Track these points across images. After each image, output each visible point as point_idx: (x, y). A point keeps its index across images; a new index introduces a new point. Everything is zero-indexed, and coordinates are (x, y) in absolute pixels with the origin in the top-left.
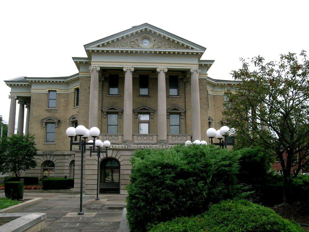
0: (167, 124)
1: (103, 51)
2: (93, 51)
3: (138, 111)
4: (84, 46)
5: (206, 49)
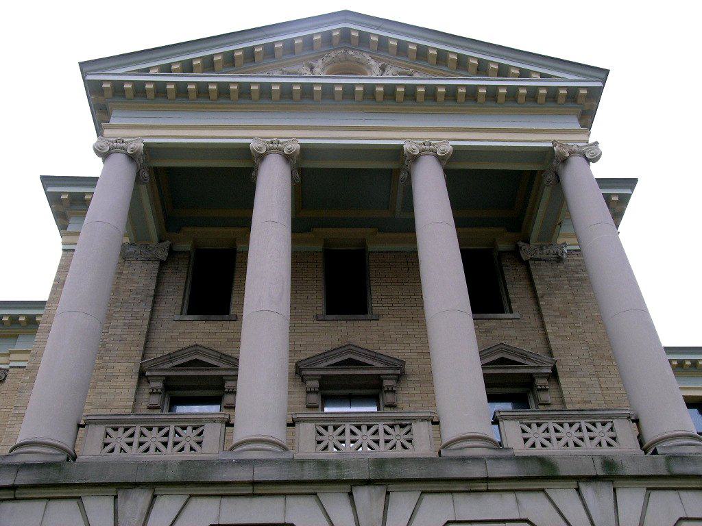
0: (363, 169)
1: (223, 90)
2: (118, 88)
3: (322, 372)
4: (83, 65)
5: (607, 72)
